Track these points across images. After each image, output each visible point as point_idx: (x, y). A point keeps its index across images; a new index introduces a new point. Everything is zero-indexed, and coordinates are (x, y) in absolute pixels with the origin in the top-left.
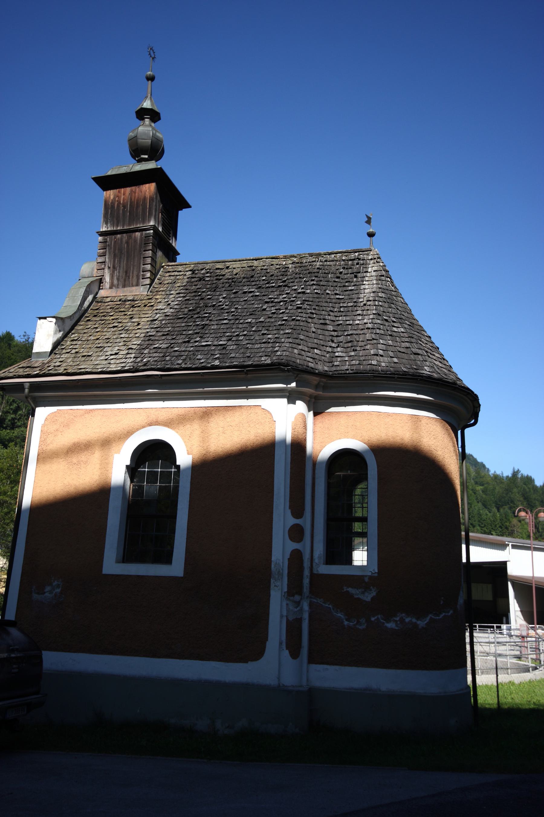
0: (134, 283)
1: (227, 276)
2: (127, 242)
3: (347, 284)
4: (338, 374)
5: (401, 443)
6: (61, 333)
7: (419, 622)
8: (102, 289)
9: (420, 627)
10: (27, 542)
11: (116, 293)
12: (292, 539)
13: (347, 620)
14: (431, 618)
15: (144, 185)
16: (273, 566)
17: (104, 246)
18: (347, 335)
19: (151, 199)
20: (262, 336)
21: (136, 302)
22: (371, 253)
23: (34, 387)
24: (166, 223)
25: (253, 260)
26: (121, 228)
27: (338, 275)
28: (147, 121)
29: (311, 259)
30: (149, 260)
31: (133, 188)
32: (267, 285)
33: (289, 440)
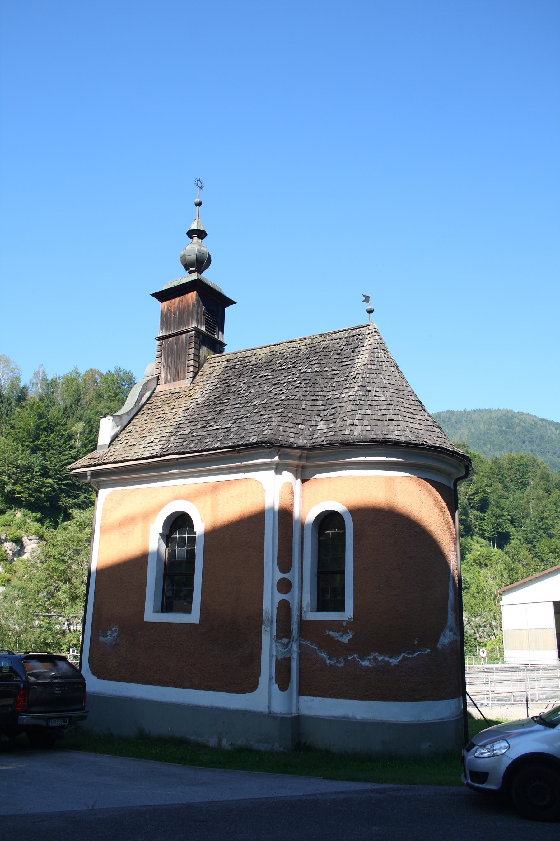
0: (182, 377)
1: (253, 363)
2: (176, 344)
3: (344, 360)
4: (315, 446)
5: (375, 502)
6: (119, 427)
7: (391, 660)
8: (159, 385)
9: (392, 664)
10: (95, 597)
11: (169, 387)
12: (280, 591)
13: (329, 659)
14: (404, 656)
15: (188, 294)
16: (264, 614)
17: (160, 349)
18: (332, 408)
19: (193, 305)
20: (260, 417)
21: (180, 394)
22: (370, 328)
23: (95, 474)
24: (210, 321)
25: (275, 345)
26: (173, 332)
27: (339, 352)
28: (195, 239)
29: (321, 339)
30: (192, 357)
31: (181, 297)
32: (280, 368)
33: (277, 508)
